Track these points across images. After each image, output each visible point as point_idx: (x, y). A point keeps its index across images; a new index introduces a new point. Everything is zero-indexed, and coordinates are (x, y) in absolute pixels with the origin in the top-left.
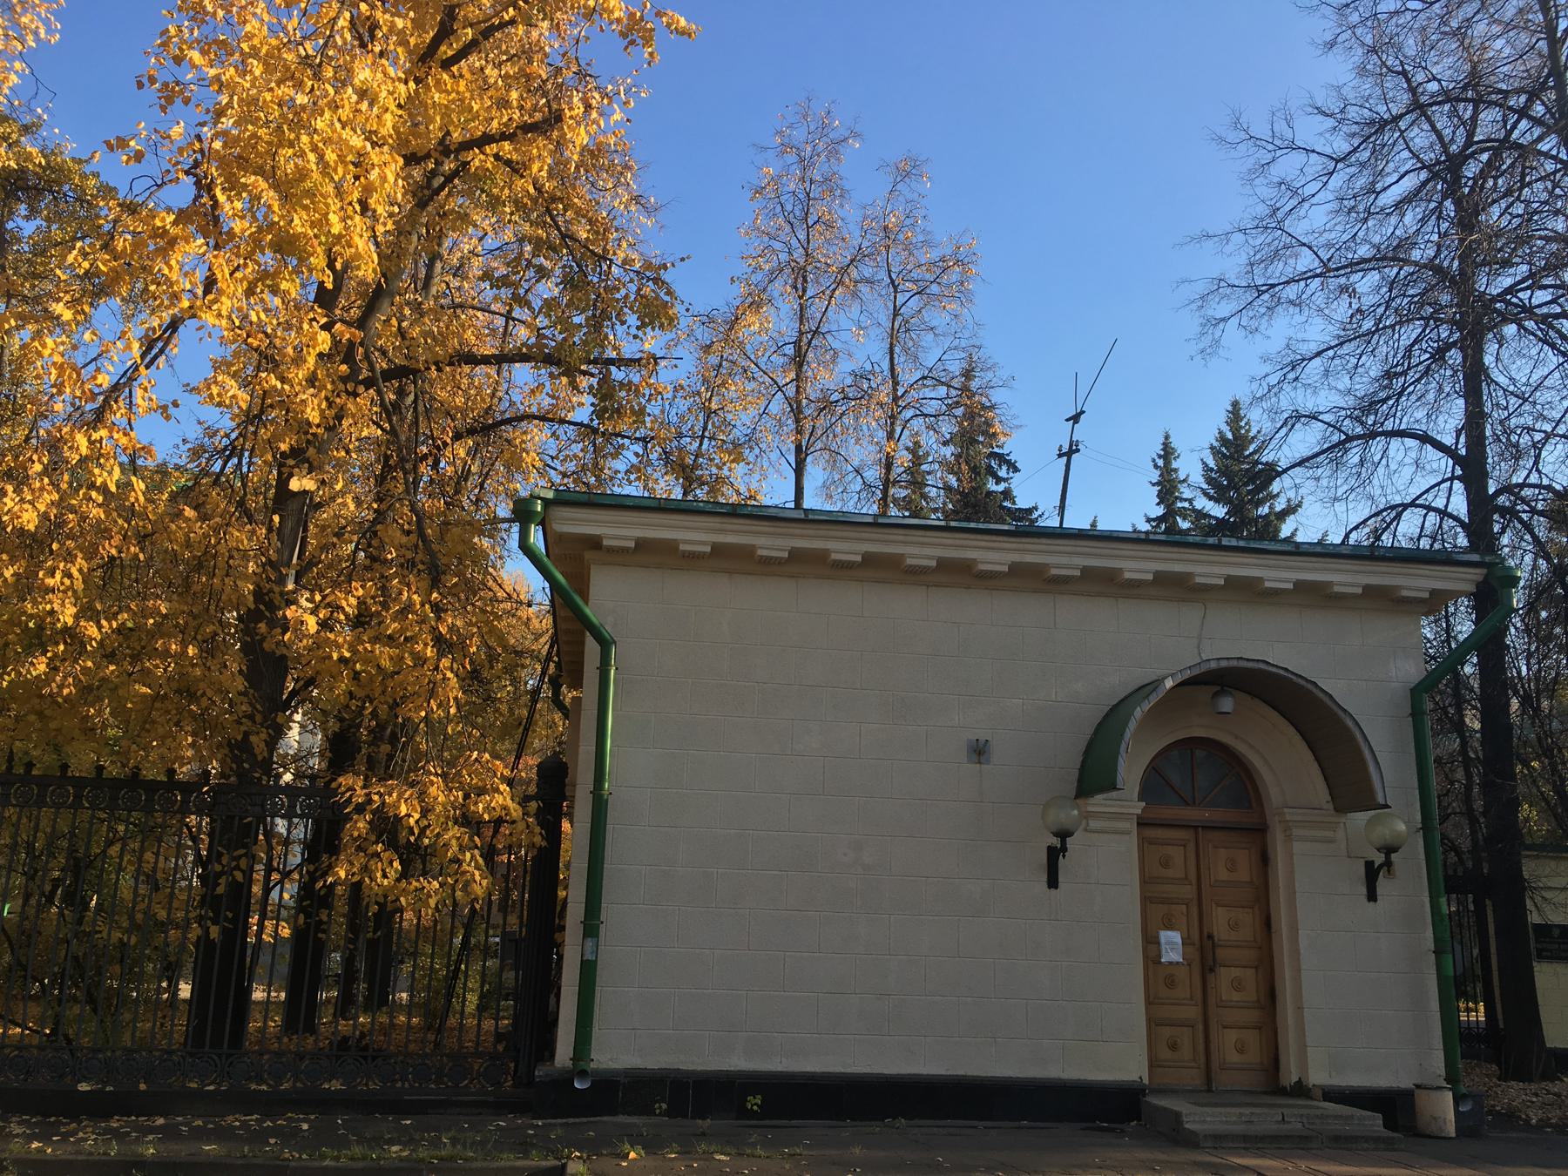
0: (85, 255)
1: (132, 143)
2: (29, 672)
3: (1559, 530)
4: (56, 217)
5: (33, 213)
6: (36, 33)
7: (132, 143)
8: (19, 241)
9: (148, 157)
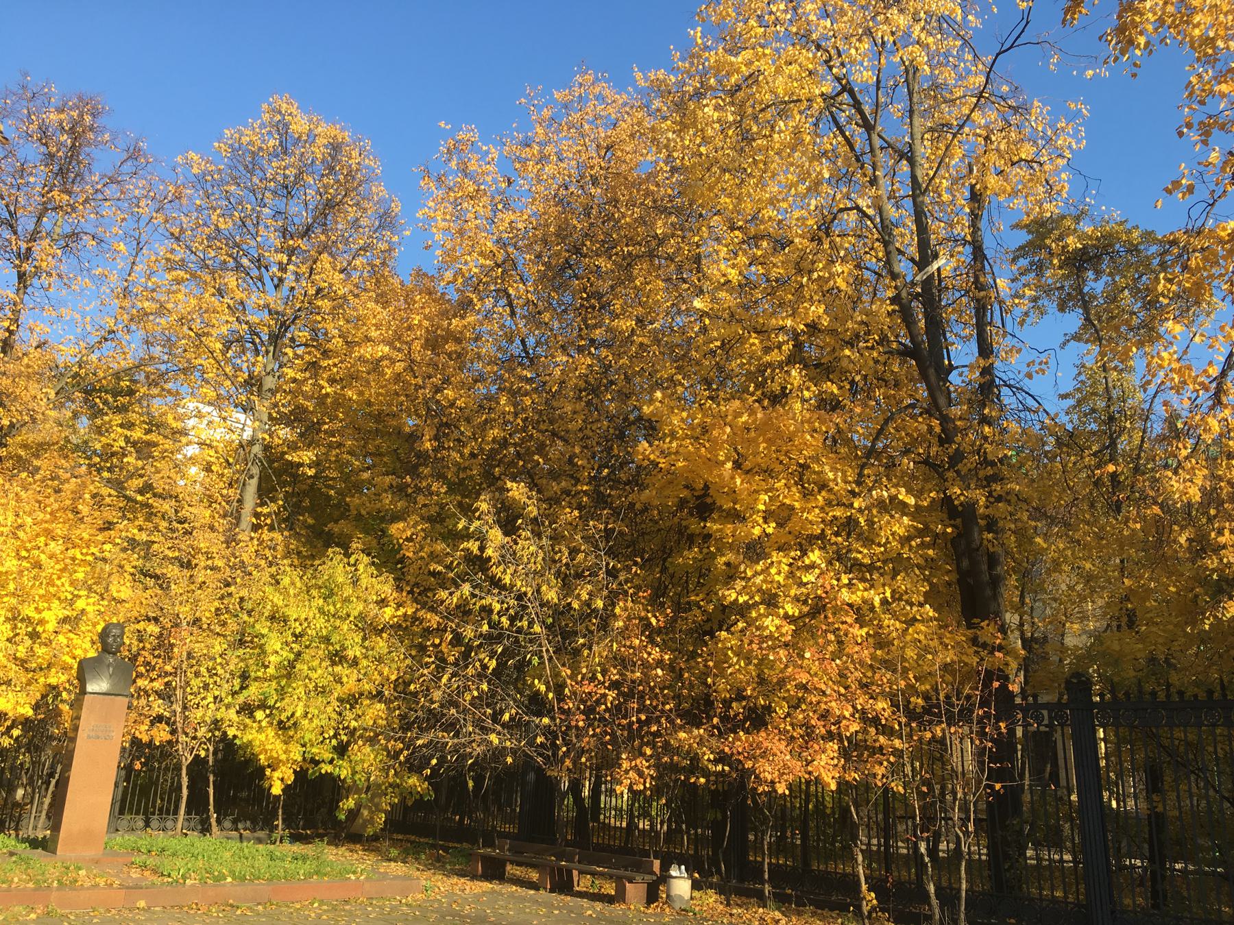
0: (1170, 281)
2: (1223, 614)
3: (845, 875)
4: (1115, 271)
5: (1098, 273)
6: (1070, 147)
7: (1184, 182)
8: (1095, 298)
9: (1199, 187)
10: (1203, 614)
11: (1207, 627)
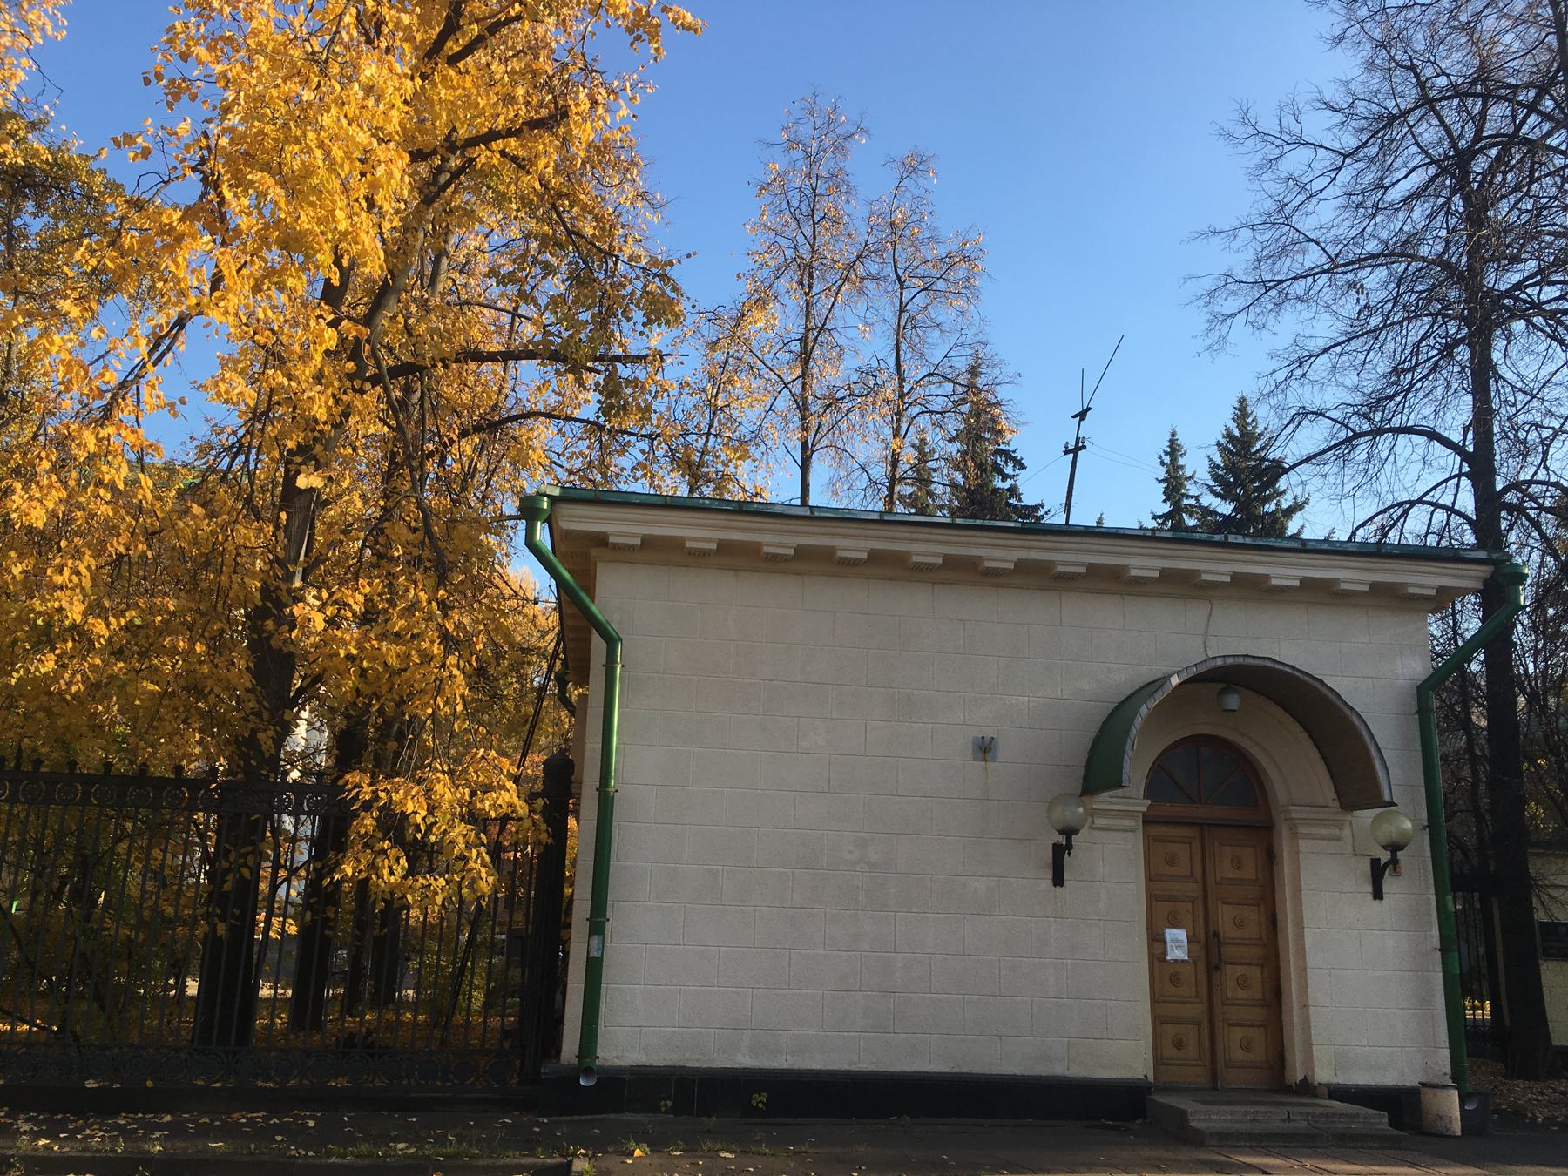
1: (139, 140)
2: (37, 669)
4: (63, 214)
5: (40, 209)
6: (43, 30)
7: (139, 140)
8: (26, 238)
9: (156, 153)
10: (13, 664)
11: (13, 681)
